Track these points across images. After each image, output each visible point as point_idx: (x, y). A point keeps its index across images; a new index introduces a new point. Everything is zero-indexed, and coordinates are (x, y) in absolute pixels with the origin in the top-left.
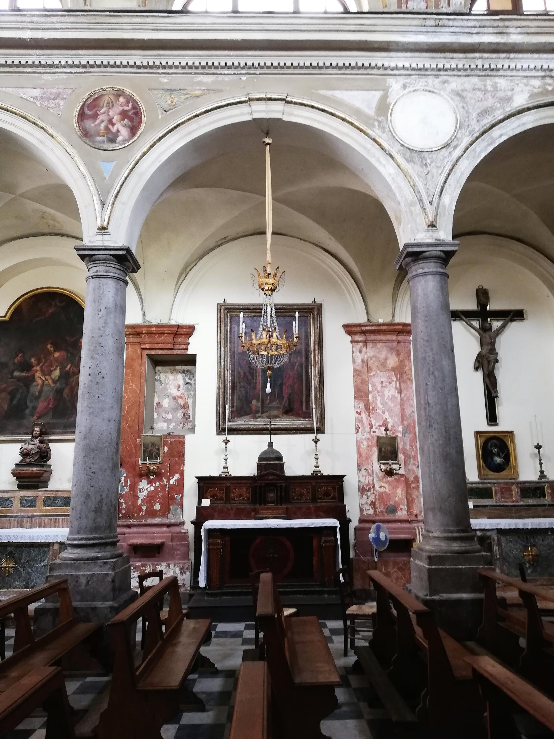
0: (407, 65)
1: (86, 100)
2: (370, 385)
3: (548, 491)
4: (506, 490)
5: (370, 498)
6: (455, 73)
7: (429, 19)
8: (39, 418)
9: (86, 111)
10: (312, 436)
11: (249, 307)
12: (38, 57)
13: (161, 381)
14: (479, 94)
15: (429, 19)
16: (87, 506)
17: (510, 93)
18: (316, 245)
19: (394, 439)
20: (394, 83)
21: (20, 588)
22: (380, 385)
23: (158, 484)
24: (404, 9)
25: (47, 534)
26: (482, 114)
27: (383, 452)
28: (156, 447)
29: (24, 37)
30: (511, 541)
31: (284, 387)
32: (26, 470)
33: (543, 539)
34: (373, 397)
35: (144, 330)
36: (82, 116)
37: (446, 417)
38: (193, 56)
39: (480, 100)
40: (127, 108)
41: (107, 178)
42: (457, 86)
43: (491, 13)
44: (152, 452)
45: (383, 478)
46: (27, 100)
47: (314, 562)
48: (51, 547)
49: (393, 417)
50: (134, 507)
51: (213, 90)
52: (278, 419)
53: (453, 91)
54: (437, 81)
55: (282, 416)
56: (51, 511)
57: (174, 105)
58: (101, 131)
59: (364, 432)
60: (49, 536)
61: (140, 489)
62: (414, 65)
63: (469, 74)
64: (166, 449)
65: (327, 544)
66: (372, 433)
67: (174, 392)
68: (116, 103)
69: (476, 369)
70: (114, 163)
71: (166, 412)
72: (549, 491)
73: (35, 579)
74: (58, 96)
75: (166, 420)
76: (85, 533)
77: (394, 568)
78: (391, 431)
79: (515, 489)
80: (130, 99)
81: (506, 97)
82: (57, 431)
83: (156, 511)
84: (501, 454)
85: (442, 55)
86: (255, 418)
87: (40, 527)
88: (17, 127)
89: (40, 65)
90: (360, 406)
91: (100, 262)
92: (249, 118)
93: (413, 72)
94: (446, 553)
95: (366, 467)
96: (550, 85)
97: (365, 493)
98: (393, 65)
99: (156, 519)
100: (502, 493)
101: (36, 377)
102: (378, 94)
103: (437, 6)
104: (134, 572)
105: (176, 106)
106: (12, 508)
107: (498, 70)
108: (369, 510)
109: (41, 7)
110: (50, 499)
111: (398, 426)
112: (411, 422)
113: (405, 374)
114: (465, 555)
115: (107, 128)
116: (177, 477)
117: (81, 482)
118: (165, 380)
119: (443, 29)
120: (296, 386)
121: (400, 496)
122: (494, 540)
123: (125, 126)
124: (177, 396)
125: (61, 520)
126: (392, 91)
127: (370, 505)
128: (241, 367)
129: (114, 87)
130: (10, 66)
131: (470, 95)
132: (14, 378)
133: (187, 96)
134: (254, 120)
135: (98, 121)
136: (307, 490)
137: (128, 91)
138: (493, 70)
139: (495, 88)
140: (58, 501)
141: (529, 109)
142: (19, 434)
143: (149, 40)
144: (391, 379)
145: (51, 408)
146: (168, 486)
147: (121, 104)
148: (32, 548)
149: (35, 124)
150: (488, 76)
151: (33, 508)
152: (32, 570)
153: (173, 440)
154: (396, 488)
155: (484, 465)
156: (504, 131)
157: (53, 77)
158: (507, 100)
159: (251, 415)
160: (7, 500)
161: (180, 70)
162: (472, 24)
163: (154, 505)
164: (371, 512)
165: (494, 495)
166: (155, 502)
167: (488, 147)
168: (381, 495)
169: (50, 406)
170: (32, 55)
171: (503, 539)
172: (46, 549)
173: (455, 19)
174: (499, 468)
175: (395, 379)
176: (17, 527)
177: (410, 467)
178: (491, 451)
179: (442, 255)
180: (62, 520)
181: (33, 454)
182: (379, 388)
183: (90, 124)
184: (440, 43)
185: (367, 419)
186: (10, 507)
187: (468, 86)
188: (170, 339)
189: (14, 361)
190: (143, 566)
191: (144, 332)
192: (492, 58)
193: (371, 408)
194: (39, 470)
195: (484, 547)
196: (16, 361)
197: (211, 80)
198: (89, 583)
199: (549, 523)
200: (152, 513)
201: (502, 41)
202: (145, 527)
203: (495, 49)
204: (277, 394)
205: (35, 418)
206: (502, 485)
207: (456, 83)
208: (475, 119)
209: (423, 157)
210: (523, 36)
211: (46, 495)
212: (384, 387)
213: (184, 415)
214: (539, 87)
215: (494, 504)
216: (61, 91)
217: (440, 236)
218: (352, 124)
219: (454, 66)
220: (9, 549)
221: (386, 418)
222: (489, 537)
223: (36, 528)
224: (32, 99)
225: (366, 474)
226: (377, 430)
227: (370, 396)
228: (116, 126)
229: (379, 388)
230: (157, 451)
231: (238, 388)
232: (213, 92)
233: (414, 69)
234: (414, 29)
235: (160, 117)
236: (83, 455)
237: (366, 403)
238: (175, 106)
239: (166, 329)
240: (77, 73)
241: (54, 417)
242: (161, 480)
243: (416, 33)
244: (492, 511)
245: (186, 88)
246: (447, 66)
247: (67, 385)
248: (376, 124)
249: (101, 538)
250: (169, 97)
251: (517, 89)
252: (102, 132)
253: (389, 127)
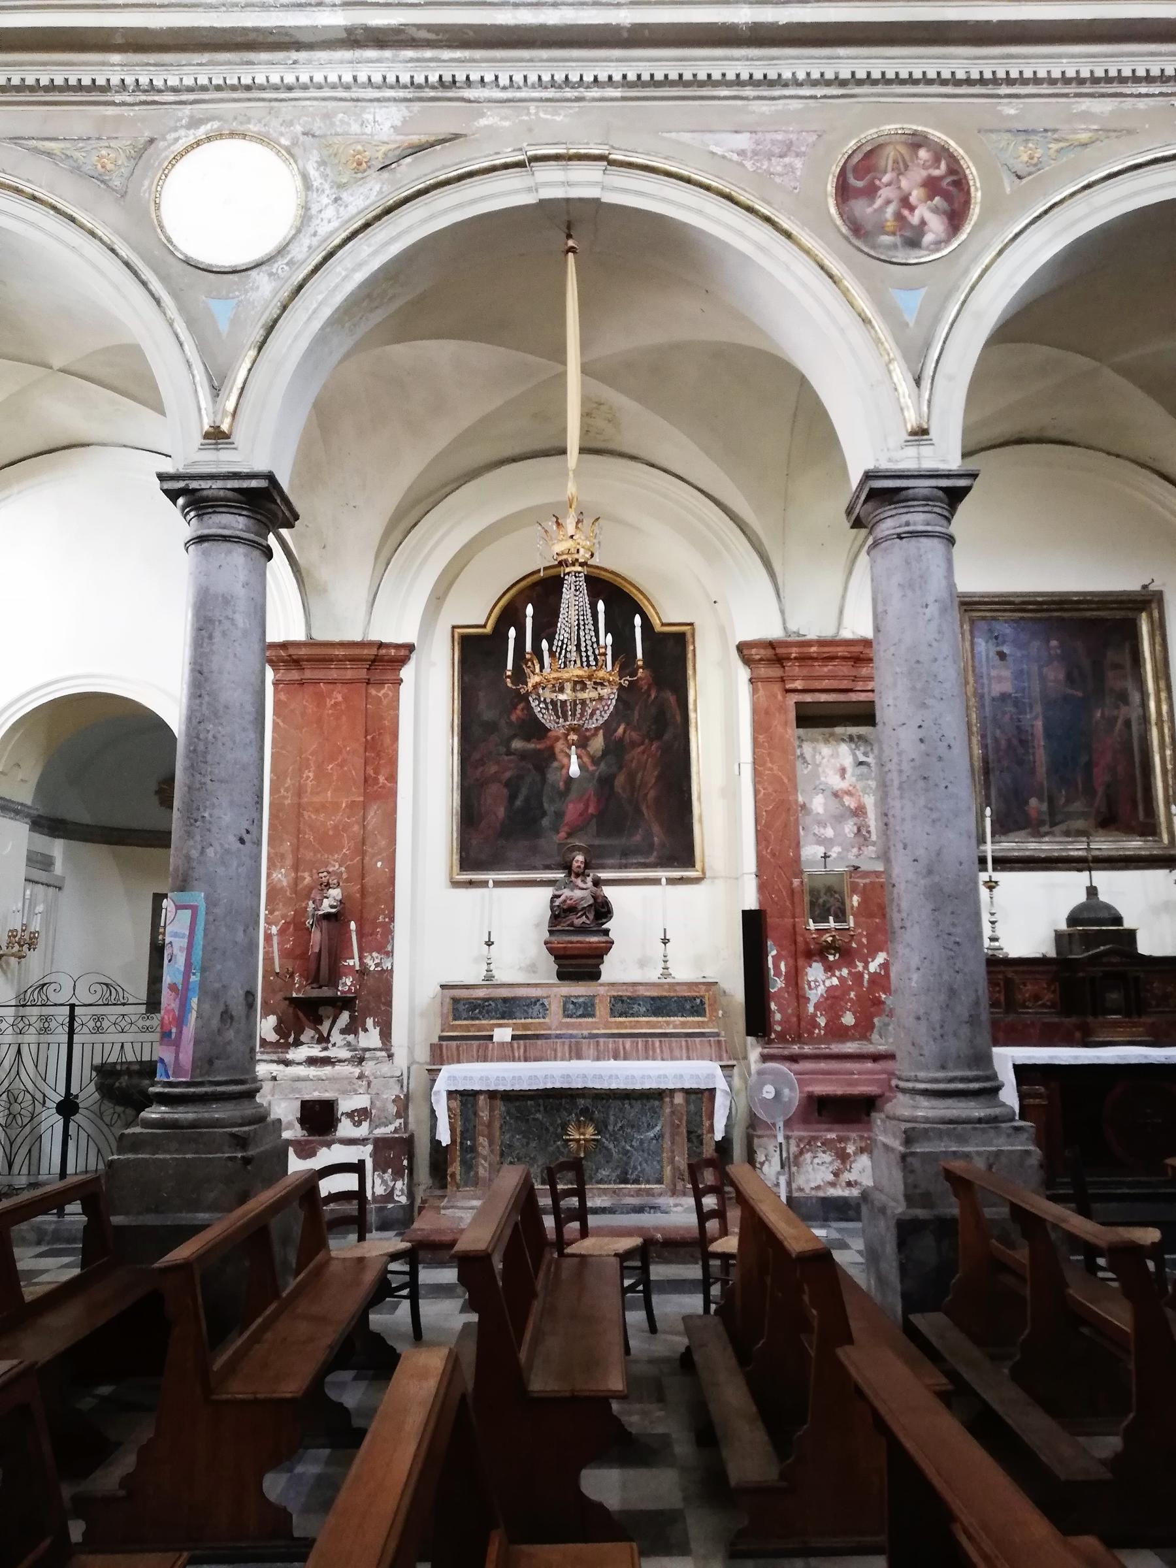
1: (849, 157)
8: (569, 835)
9: (852, 181)
11: (1012, 599)
12: (748, 63)
13: (804, 758)
16: (953, 1011)
18: (1143, 465)
21: (610, 1183)
23: (845, 972)
25: (661, 1072)
28: (837, 896)
29: (736, 21)
31: (1095, 770)
32: (578, 942)
35: (794, 652)
36: (844, 191)
40: (936, 173)
41: (911, 325)
44: (828, 905)
46: (724, 157)
48: (667, 1099)
50: (799, 1019)
51: (1115, 131)
55: (1097, 831)
56: (626, 1024)
57: (1035, 165)
58: (889, 224)
60: (665, 1076)
61: (809, 983)
64: (856, 900)
67: (835, 782)
68: (912, 161)
70: (923, 291)
71: (822, 824)
73: (640, 1165)
74: (788, 148)
75: (821, 841)
76: (957, 1067)
80: (942, 153)
82: (610, 861)
83: (847, 1028)
86: (1038, 834)
87: (616, 1058)
88: (708, 217)
89: (752, 82)
91: (916, 503)
92: (529, 199)
99: (849, 1044)
101: (557, 750)
104: (824, 1152)
105: (1039, 167)
106: (547, 1020)
110: (623, 1002)
115: (899, 217)
116: (881, 958)
117: (932, 963)
118: (814, 756)
123: (935, 210)
124: (841, 790)
125: (657, 1044)
128: (999, 727)
129: (905, 126)
130: (32, 89)
132: (514, 754)
133: (1062, 145)
134: (543, 203)
135: (879, 202)
137: (937, 135)
140: (639, 1005)
142: (533, 868)
143: (1000, 22)
145: (592, 815)
146: (866, 976)
147: (922, 166)
148: (626, 1101)
149: (750, 209)
151: (590, 1020)
152: (632, 1146)
153: (867, 881)
157: (773, 108)
159: (1027, 831)
160: (535, 1004)
161: (1045, 89)
163: (842, 1016)
166: (844, 1010)
169: (591, 810)
170: (738, 60)
172: (657, 1103)
176: (570, 1059)
179: (940, 493)
180: (525, 1047)
181: (584, 908)
183: (863, 209)
186: (544, 1018)
188: (845, 669)
189: (509, 718)
190: (841, 1139)
191: (793, 655)
194: (603, 943)
196: (513, 718)
197: (1110, 108)
198: (993, 1170)
200: (838, 1032)
202: (829, 1061)
205: (563, 834)
211: (616, 994)
213: (859, 830)
216: (793, 137)
220: (581, 1102)
223: (609, 1059)
224: (735, 155)
228: (917, 212)
230: (838, 904)
231: (997, 773)
232: (1116, 134)
235: (1008, 190)
236: (930, 906)
238: (1038, 166)
239: (839, 649)
240: (825, 97)
241: (598, 834)
242: (851, 964)
245: (1058, 127)
247: (620, 768)
249: (936, 1081)
250: (1022, 148)
252: (890, 224)
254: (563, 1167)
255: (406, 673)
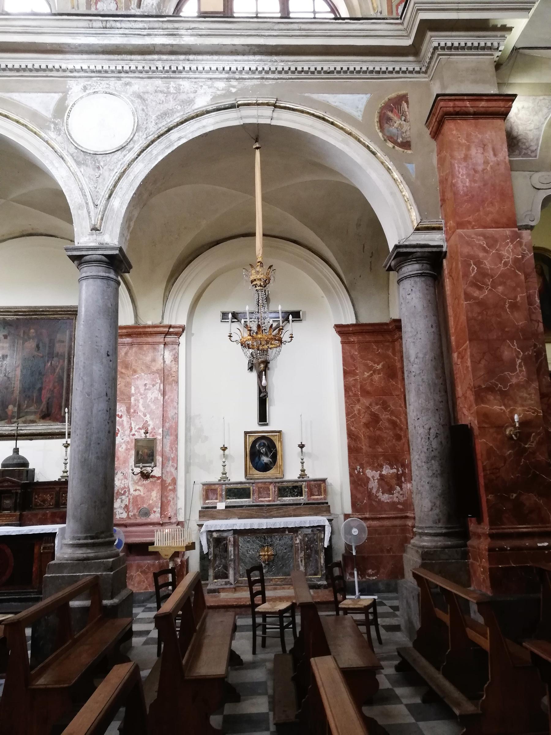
0: (85, 67)
2: (133, 388)
3: (305, 490)
4: (263, 490)
5: (124, 502)
6: (137, 75)
7: (95, 20)
10: (64, 441)
14: (161, 96)
15: (95, 20)
17: (192, 96)
19: (153, 441)
20: (74, 85)
22: (144, 388)
24: (93, 11)
26: (162, 118)
27: (140, 455)
30: (248, 542)
33: (280, 539)
34: (135, 400)
37: (89, 423)
38: (316, 61)
39: (161, 102)
42: (139, 89)
43: (204, 15)
45: (139, 481)
47: (34, 569)
49: (154, 420)
52: (34, 424)
53: (134, 93)
54: (119, 83)
59: (124, 436)
62: (92, 67)
63: (151, 76)
65: (46, 551)
66: (131, 436)
69: (251, 369)
72: (306, 490)
77: (137, 571)
78: (150, 433)
79: (272, 490)
81: (188, 99)
84: (268, 453)
85: (119, 57)
90: (122, 409)
93: (93, 75)
94: (67, 560)
95: (122, 470)
96: (234, 87)
97: (120, 497)
98: (70, 67)
100: (260, 492)
102: (57, 97)
103: (127, 8)
107: (180, 72)
108: (122, 513)
109: (28, 11)
111: (159, 428)
112: (173, 424)
113: (170, 376)
114: (85, 562)
119: (112, 31)
120: (56, 390)
121: (155, 499)
122: (230, 541)
126: (71, 93)
127: (124, 508)
131: (151, 97)
134: (244, 126)
136: (50, 496)
138: (174, 72)
139: (178, 90)
141: (208, 112)
144: (155, 381)
150: (171, 78)
154: (150, 490)
155: (251, 465)
156: (182, 134)
158: (188, 102)
159: (6, 421)
162: (141, 25)
164: (124, 515)
165: (251, 494)
167: (166, 150)
168: (135, 498)
171: (241, 539)
173: (122, 21)
174: (265, 468)
175: (159, 381)
177: (168, 470)
178: (259, 451)
179: (104, 258)
182: (142, 390)
184: (113, 45)
185: (128, 422)
187: (150, 88)
192: (171, 60)
193: (132, 411)
195: (220, 549)
199: (259, 524)
201: (174, 43)
203: (174, 51)
204: (35, 399)
206: (260, 485)
207: (138, 85)
208: (153, 122)
209: (97, 160)
210: (196, 38)
212: (148, 389)
214: (223, 90)
215: (251, 504)
217: (104, 240)
218: (26, 126)
219: (133, 68)
221: (146, 421)
222: (225, 539)
225: (122, 477)
226: (136, 433)
227: (133, 399)
229: (142, 390)
233: (93, 72)
234: (83, 30)
237: (128, 406)
243: (86, 35)
244: (243, 511)
246: (126, 68)
248: (52, 126)
251: (201, 91)
253: (64, 129)
254: (253, 569)
255: (182, 339)
